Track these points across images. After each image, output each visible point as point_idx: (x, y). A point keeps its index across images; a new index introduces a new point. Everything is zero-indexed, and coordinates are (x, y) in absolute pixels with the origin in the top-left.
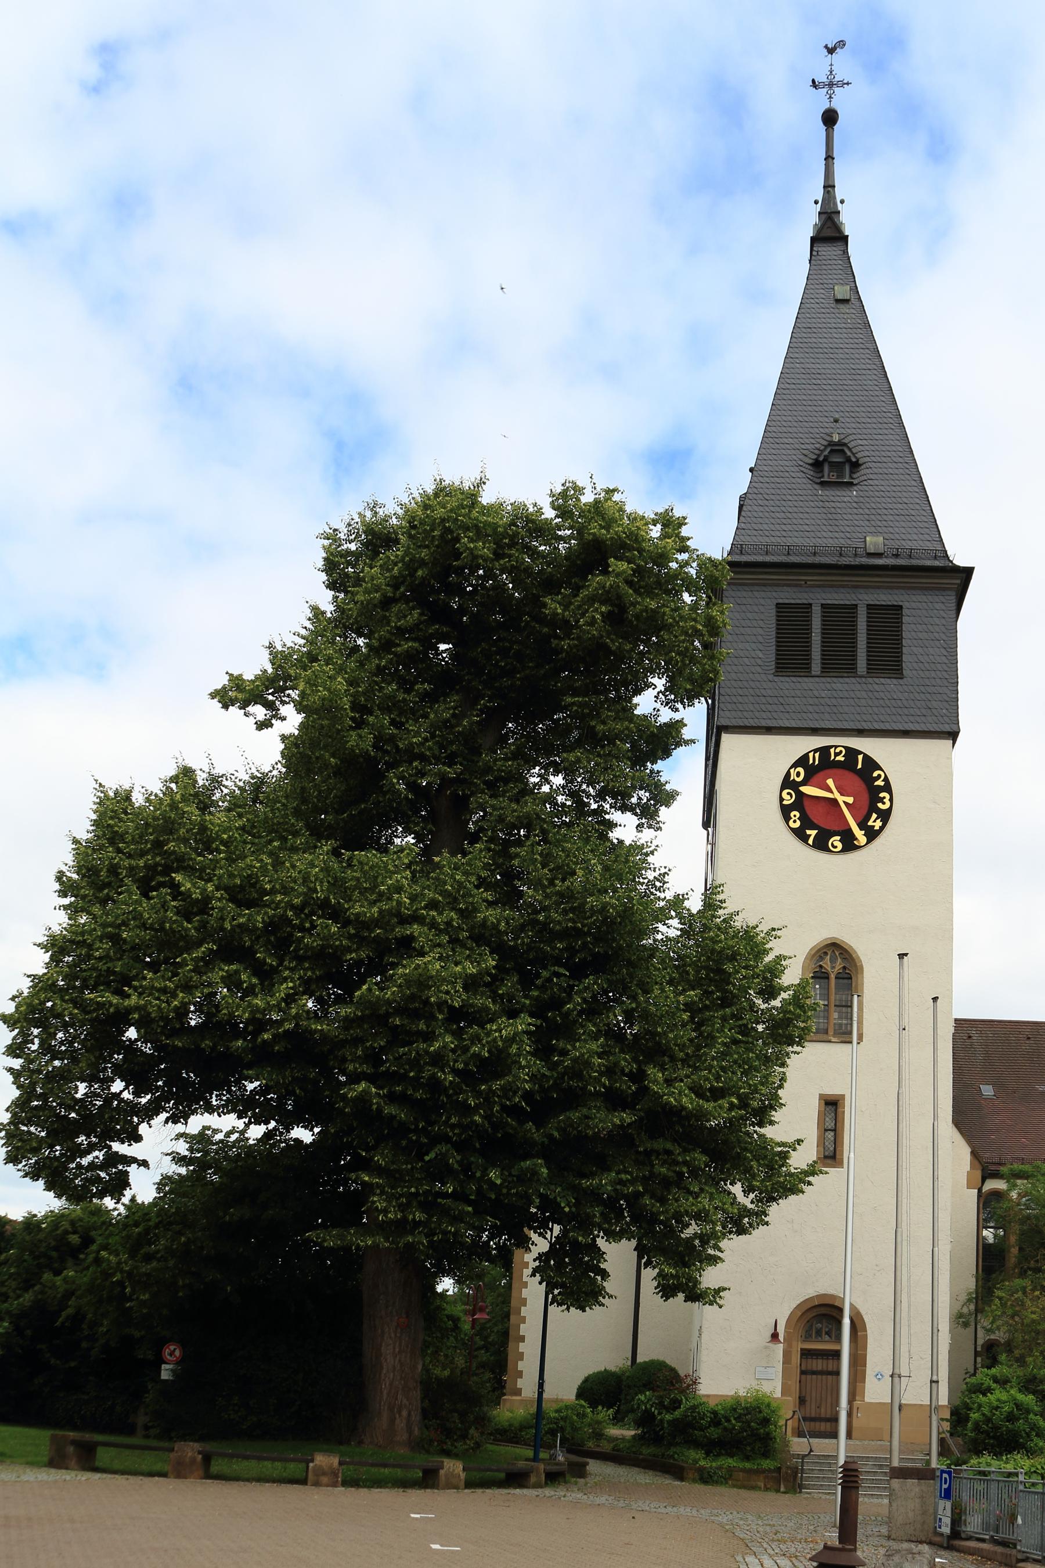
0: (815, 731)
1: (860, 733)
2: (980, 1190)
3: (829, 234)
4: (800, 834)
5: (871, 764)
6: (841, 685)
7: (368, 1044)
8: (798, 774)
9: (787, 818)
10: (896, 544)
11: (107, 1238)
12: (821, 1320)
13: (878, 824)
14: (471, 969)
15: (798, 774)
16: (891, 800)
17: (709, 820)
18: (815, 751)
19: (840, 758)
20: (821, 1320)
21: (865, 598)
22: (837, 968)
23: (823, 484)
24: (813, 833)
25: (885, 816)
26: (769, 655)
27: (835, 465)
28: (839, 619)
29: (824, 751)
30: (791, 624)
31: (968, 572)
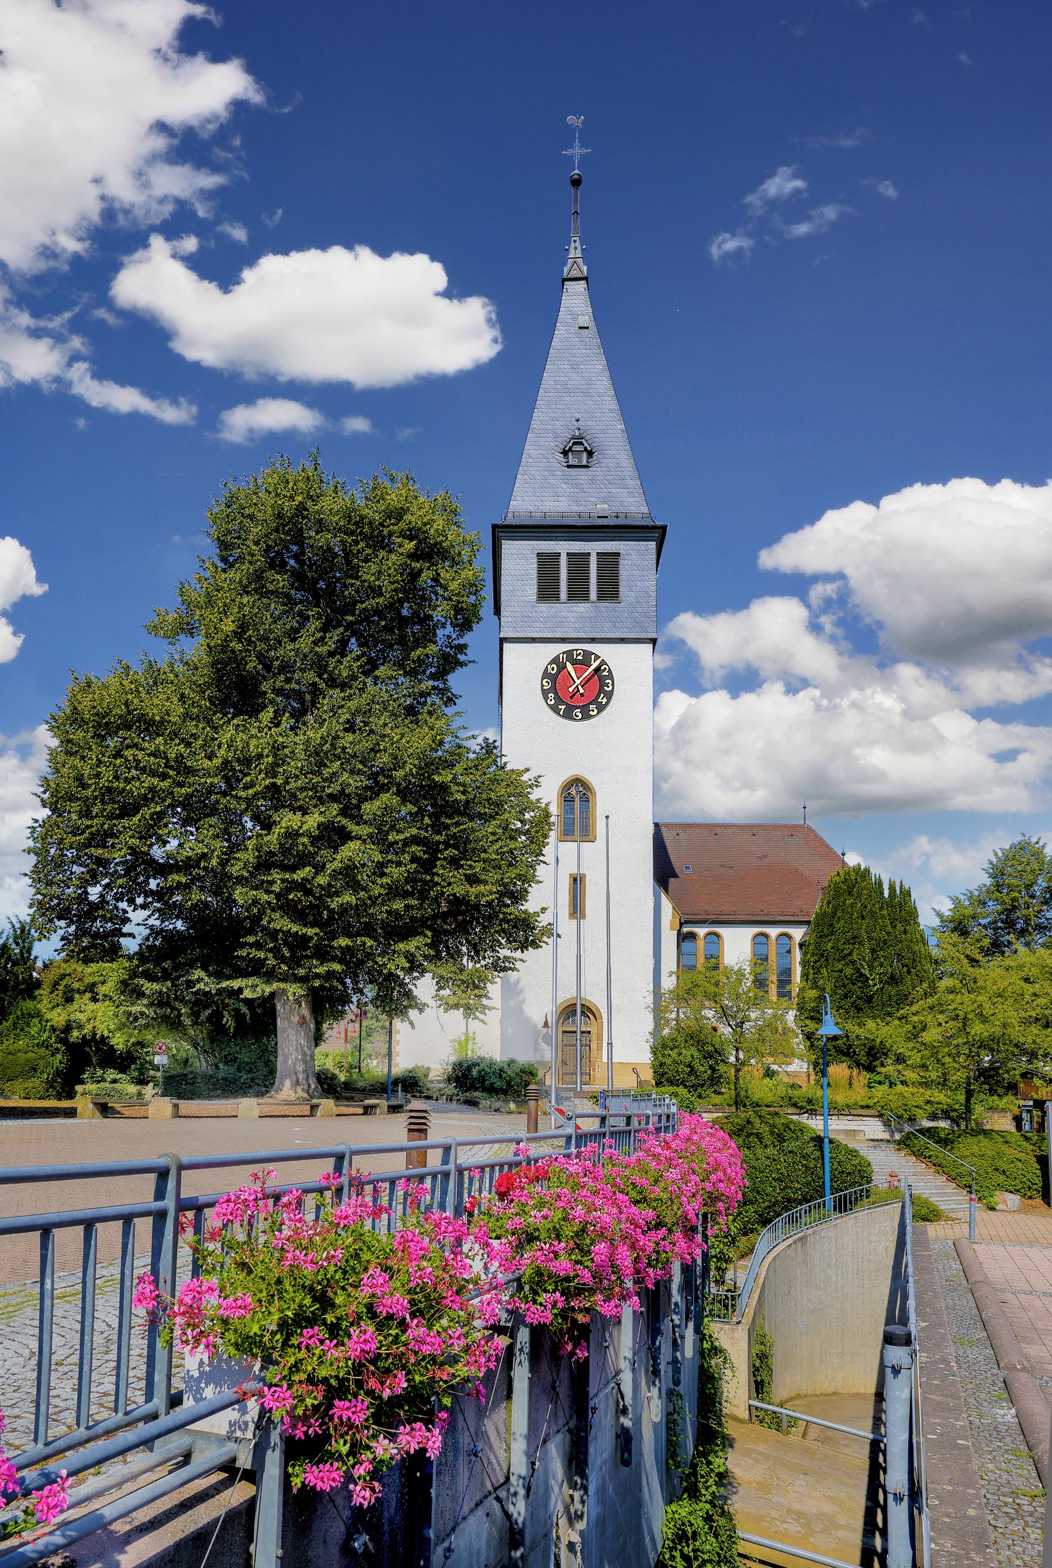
0: (563, 640)
1: (593, 640)
2: (679, 931)
4: (555, 709)
6: (581, 608)
7: (239, 647)
8: (553, 669)
9: (546, 698)
10: (616, 509)
12: (576, 1013)
13: (605, 701)
15: (553, 669)
16: (613, 685)
18: (564, 653)
19: (580, 657)
20: (576, 1013)
21: (594, 548)
22: (578, 792)
23: (569, 466)
25: (609, 695)
28: (579, 561)
30: (547, 564)
31: (664, 528)
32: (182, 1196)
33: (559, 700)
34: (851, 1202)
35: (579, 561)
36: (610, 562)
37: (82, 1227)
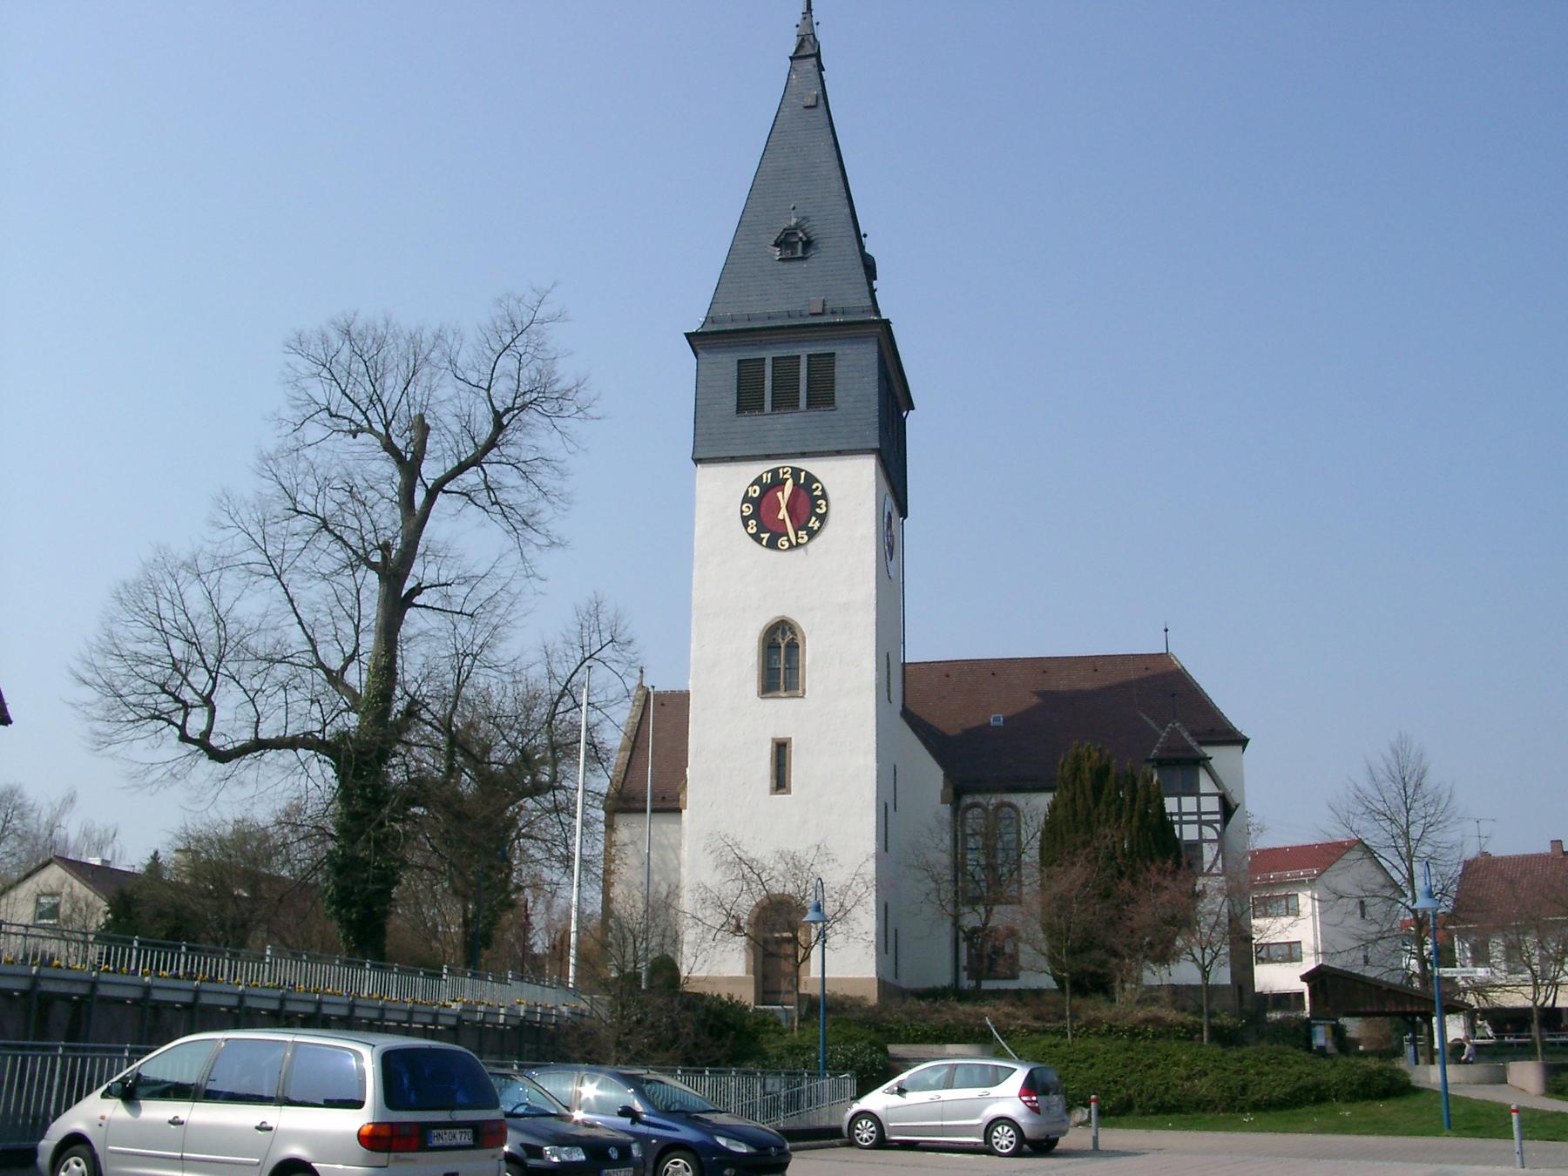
0: (768, 457)
1: (803, 455)
3: (807, 52)
4: (756, 538)
5: (811, 479)
6: (787, 419)
9: (746, 526)
11: (186, 707)
14: (1518, 999)
17: (890, 546)
21: (803, 352)
24: (766, 536)
25: (822, 518)
26: (732, 401)
27: (795, 244)
28: (786, 368)
29: (775, 472)
32: (918, 651)
33: (761, 528)
34: (91, 1079)
35: (786, 368)
36: (823, 368)
37: (747, 995)
